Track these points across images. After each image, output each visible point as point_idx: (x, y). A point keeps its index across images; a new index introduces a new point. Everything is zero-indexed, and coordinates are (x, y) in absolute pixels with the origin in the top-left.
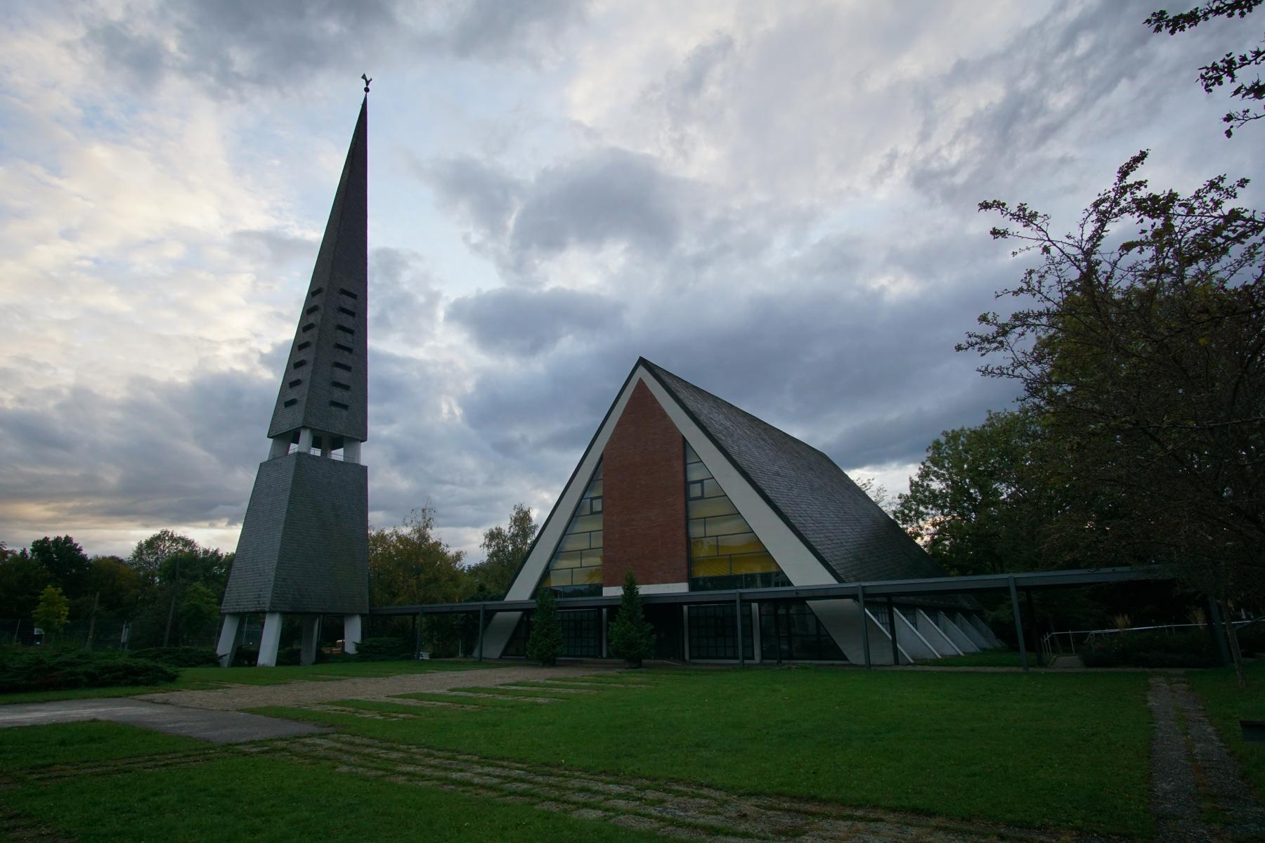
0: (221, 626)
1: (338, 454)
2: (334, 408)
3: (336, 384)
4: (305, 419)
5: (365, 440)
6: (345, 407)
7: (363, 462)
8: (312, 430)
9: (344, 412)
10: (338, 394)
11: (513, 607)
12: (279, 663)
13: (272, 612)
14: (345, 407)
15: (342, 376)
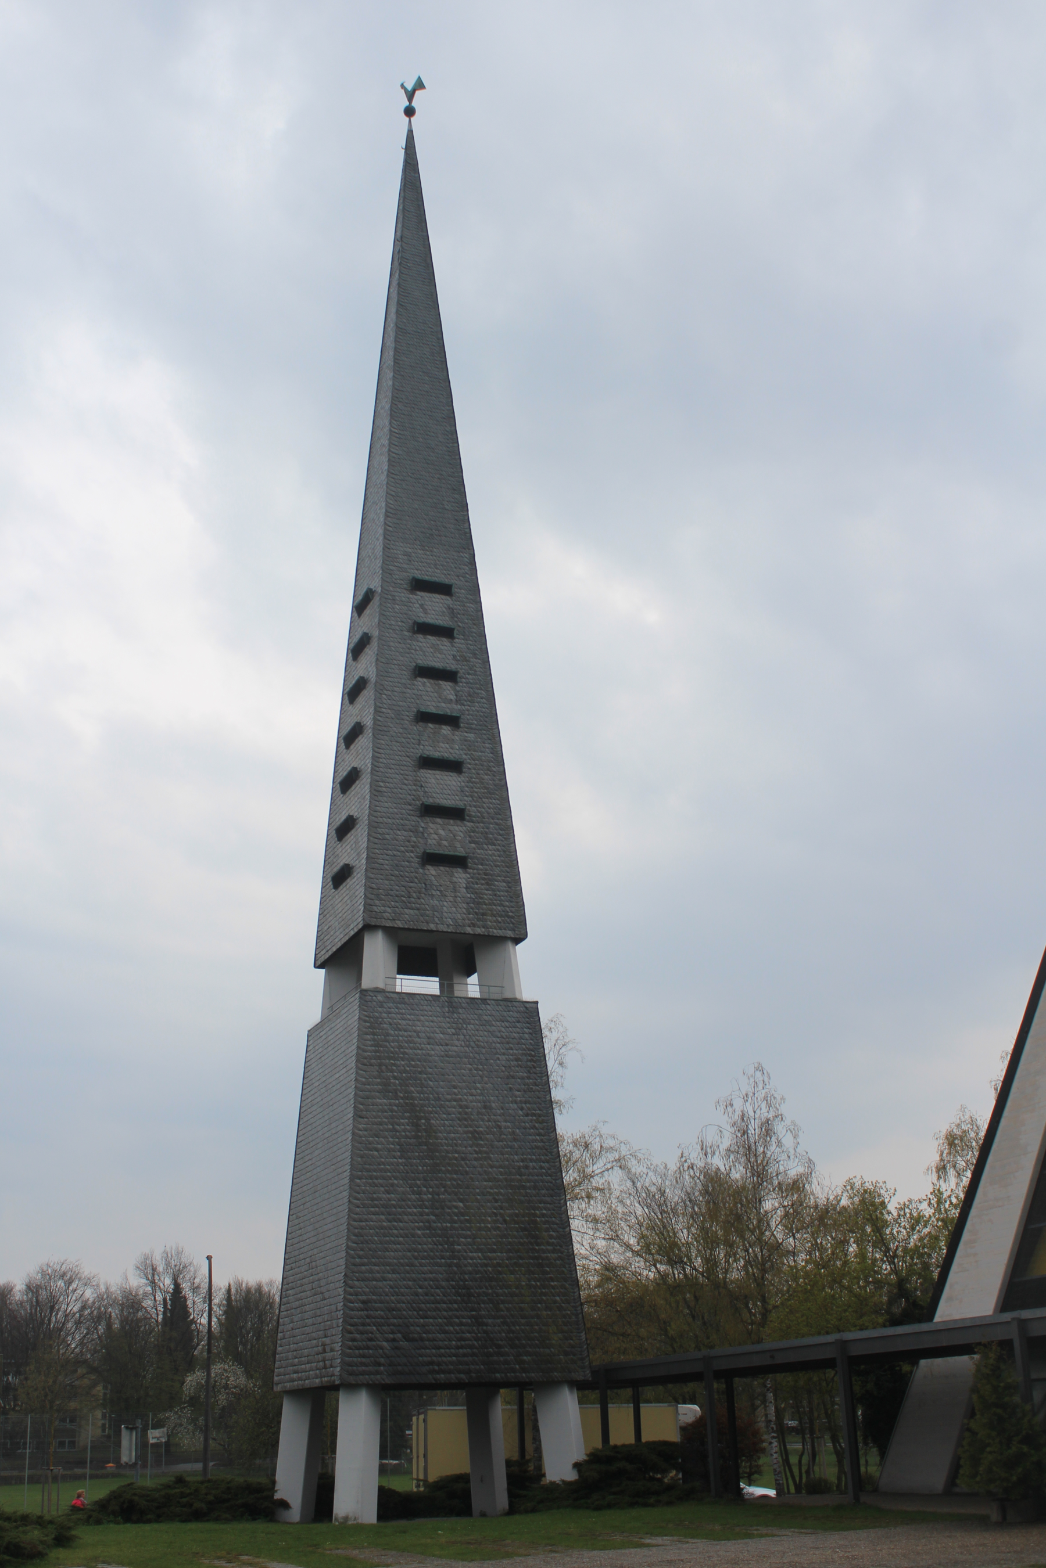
0: (279, 1414)
1: (472, 987)
2: (432, 870)
3: (431, 811)
4: (368, 907)
5: (518, 941)
6: (458, 862)
7: (526, 994)
8: (391, 932)
9: (460, 876)
10: (441, 835)
11: (960, 1341)
12: (381, 1517)
13: (352, 1387)
14: (458, 862)
15: (443, 788)
